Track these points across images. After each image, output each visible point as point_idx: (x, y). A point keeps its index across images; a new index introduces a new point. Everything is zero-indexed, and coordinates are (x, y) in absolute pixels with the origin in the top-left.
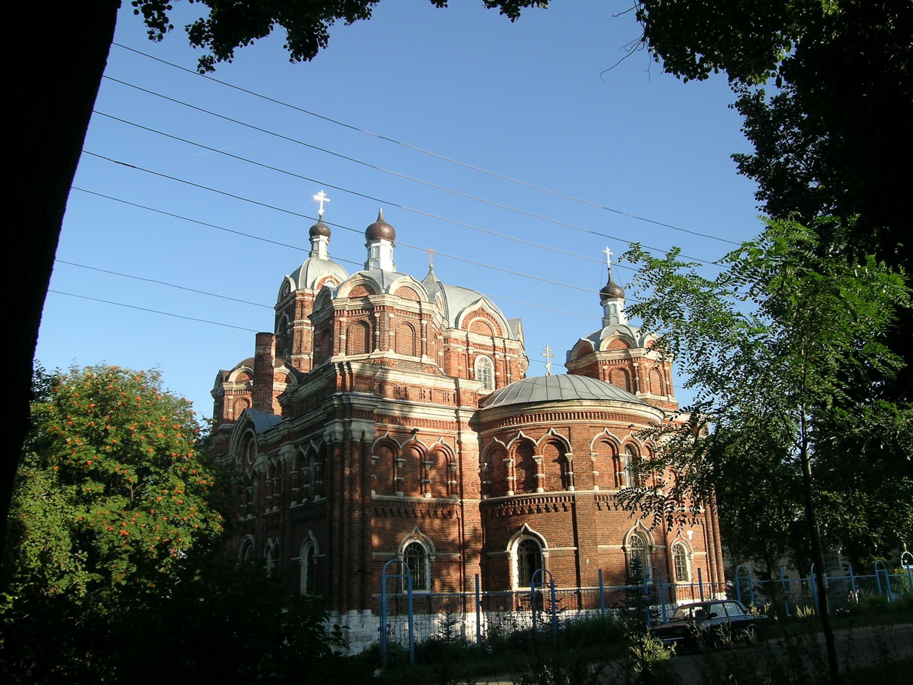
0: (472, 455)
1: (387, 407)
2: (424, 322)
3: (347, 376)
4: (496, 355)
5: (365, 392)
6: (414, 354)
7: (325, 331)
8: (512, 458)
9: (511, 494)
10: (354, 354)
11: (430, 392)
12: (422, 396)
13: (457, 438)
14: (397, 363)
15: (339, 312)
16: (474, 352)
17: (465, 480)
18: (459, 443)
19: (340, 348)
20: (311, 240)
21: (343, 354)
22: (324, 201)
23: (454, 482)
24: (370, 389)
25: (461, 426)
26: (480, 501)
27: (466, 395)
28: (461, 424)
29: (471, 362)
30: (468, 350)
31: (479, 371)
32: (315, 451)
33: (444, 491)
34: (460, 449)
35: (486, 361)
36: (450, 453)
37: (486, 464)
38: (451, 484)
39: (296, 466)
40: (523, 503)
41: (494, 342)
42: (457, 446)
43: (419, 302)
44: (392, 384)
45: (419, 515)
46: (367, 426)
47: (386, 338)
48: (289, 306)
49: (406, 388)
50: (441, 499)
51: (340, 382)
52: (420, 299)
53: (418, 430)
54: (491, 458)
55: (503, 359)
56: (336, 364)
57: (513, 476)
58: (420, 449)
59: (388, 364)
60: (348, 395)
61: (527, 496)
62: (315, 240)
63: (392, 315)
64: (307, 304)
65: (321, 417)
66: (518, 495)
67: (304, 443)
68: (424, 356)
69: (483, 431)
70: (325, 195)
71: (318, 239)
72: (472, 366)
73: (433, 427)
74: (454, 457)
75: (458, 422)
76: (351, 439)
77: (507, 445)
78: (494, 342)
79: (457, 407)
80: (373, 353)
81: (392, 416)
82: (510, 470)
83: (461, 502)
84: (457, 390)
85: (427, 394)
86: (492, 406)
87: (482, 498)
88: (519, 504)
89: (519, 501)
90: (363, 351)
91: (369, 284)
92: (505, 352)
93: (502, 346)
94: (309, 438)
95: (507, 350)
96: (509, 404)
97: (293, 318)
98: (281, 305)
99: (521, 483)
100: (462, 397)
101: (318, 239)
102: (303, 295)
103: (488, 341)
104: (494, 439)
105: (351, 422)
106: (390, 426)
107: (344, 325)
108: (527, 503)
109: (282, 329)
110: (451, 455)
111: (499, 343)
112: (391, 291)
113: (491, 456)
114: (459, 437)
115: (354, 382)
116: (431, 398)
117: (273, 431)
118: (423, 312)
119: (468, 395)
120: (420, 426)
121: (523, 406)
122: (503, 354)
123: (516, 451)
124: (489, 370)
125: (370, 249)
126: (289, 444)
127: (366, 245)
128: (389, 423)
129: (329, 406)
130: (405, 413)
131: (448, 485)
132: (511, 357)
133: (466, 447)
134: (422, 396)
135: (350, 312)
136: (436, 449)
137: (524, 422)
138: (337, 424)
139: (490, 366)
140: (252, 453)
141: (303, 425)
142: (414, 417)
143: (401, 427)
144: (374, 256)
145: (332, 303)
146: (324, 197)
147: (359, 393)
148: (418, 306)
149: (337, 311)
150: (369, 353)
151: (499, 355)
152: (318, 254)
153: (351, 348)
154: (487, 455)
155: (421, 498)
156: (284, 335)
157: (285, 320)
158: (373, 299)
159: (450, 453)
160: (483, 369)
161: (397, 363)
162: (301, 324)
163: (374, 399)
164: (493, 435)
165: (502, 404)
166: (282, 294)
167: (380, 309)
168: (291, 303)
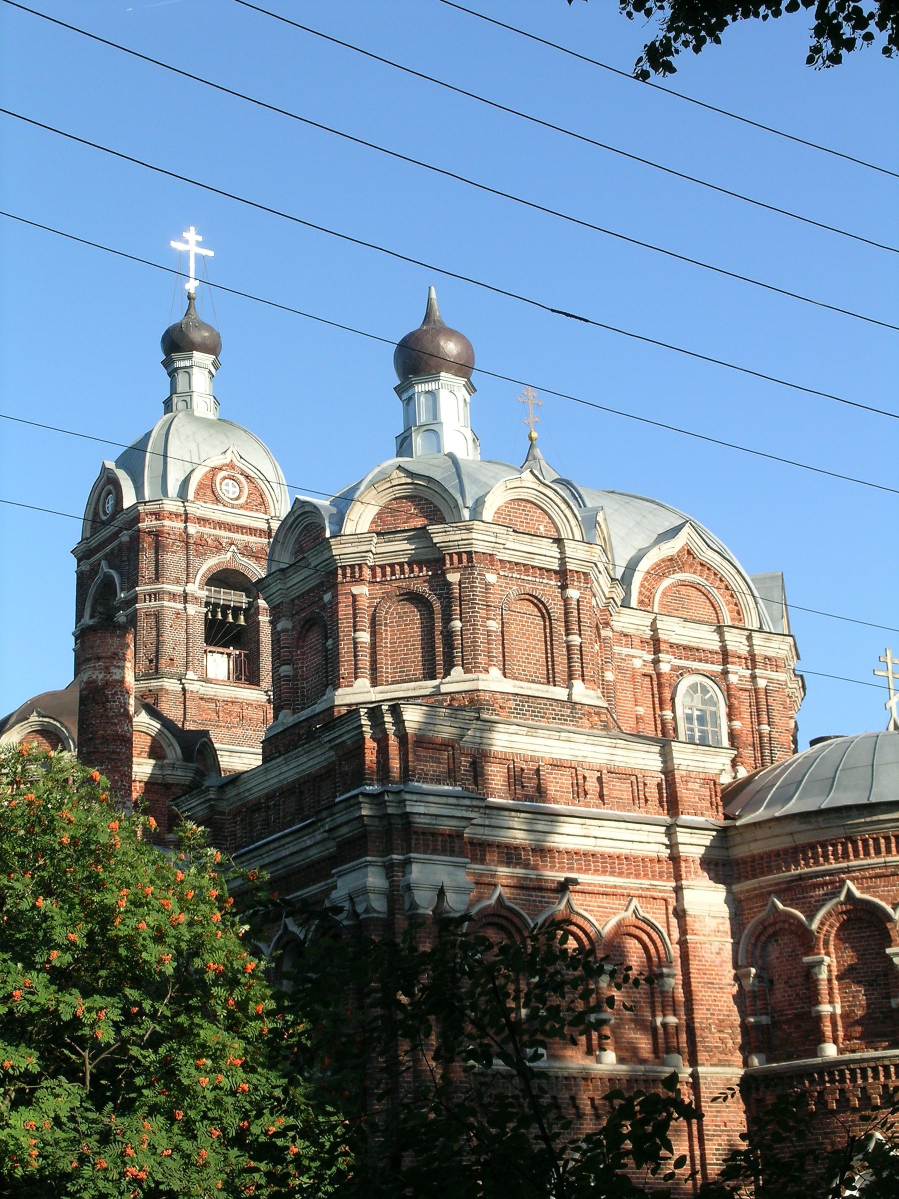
0: (715, 948)
1: (494, 822)
2: (573, 593)
3: (393, 741)
4: (730, 676)
5: (438, 782)
6: (551, 679)
7: (307, 621)
8: (828, 954)
9: (830, 1051)
10: (393, 683)
11: (600, 779)
12: (579, 791)
13: (673, 903)
14: (512, 704)
15: (349, 571)
16: (675, 668)
17: (700, 1015)
18: (680, 914)
20: (167, 363)
21: (363, 683)
22: (198, 257)
23: (672, 1020)
24: (451, 776)
25: (683, 869)
26: (741, 1072)
27: (690, 785)
28: (683, 864)
29: (667, 694)
30: (656, 662)
31: (689, 718)
33: (644, 1044)
34: (683, 931)
35: (705, 690)
36: (658, 941)
37: (753, 970)
38: (665, 1025)
40: (865, 1077)
41: (722, 640)
42: (674, 921)
43: (559, 541)
44: (503, 760)
45: (588, 1110)
46: (449, 874)
47: (481, 638)
49: (538, 770)
50: (642, 1068)
51: (374, 758)
52: (558, 530)
53: (575, 882)
54: (764, 956)
55: (748, 686)
56: (363, 711)
57: (831, 1002)
58: (580, 934)
59: (489, 706)
60: (398, 793)
61: (878, 1059)
62: (179, 364)
63: (491, 578)
65: (313, 852)
66: (848, 1056)
68: (578, 684)
69: (739, 880)
70: (200, 238)
71: (188, 363)
72: (668, 706)
73: (612, 873)
74: (667, 952)
75: (675, 859)
76: (409, 909)
77: (811, 917)
78: (722, 640)
79: (667, 819)
80: (448, 679)
81: (508, 847)
82: (824, 987)
83: (695, 1076)
84: (668, 772)
85: (592, 785)
86: (760, 814)
87: (746, 1063)
88: (854, 1079)
89: (853, 1072)
90: (419, 673)
91: (427, 494)
92: (754, 667)
93: (743, 650)
95: (759, 659)
96: (814, 808)
97: (132, 580)
98: (94, 543)
99: (858, 1023)
100: (682, 792)
101: (188, 363)
102: (158, 515)
103: (707, 639)
104: (774, 906)
105: (408, 862)
106: (503, 871)
107: (363, 603)
108: (876, 1077)
109: (100, 609)
110: (661, 948)
111: (736, 642)
112: (488, 514)
113: (764, 948)
114: (679, 898)
115: (411, 757)
116: (601, 796)
118: (570, 567)
119: (697, 786)
120: (579, 870)
121: (854, 813)
122: (748, 673)
123: (837, 935)
124: (715, 715)
125: (410, 398)
127: (400, 390)
128: (501, 863)
129: (346, 823)
130: (540, 836)
131: (654, 1029)
132: (770, 680)
133: (697, 926)
134: (579, 791)
135: (378, 570)
136: (621, 931)
137: (857, 856)
138: (370, 869)
139: (715, 704)
142: (562, 847)
143: (532, 874)
144: (423, 417)
145: (329, 548)
146: (199, 244)
147: (425, 786)
148: (554, 551)
149: (344, 568)
150: (433, 677)
151: (738, 674)
152: (188, 405)
153: (386, 667)
154: (755, 945)
155: (589, 1063)
157: (108, 587)
158: (440, 535)
159: (658, 941)
160: (696, 713)
161: (512, 704)
162: (156, 595)
163: (467, 802)
164: (769, 894)
165: (793, 806)
167: (460, 561)
168: (125, 537)
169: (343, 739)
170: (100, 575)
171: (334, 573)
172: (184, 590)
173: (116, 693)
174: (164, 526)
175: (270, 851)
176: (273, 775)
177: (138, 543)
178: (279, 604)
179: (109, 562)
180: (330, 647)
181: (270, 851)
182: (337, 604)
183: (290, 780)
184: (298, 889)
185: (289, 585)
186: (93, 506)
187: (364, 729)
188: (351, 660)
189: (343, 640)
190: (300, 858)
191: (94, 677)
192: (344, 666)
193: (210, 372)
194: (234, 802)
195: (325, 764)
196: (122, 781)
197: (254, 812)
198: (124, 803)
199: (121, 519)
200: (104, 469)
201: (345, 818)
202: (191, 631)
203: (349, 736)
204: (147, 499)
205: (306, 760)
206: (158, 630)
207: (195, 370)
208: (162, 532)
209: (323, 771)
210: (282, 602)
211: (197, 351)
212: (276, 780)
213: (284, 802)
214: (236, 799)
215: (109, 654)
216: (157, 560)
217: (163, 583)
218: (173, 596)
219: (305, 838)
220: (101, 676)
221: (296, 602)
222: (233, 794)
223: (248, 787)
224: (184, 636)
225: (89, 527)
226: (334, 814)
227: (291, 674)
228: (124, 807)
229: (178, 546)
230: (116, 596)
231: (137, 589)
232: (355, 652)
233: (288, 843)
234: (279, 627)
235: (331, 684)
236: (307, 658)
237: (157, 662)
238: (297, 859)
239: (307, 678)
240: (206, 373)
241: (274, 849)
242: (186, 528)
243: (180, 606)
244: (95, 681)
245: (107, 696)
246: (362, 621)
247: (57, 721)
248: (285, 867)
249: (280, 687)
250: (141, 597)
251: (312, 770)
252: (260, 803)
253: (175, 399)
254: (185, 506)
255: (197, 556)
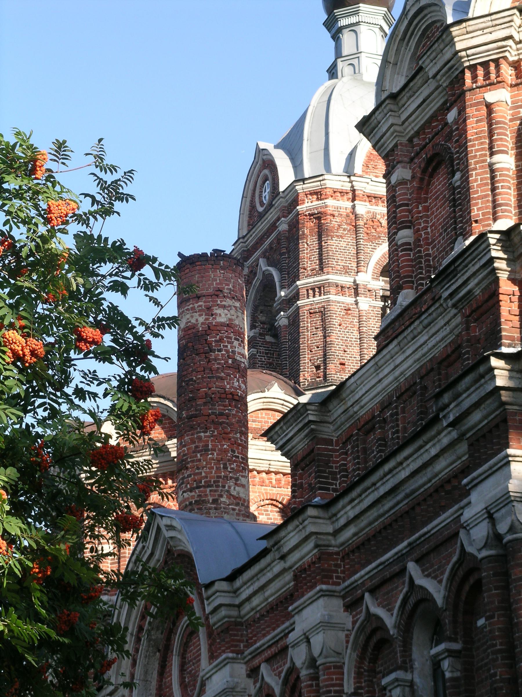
7: (429, 161)
19: (495, 205)
32: (433, 600)
39: (359, 675)
48: (278, 239)
62: (343, 22)
64: (334, 222)
65: (441, 464)
67: (384, 582)
71: (353, 20)
94: (402, 558)
98: (251, 241)
101: (353, 20)
102: (318, 194)
109: (262, 318)
117: (263, 563)
126: (324, 594)
129: (476, 405)
140: (190, 668)
141: (373, 513)
145: (451, 42)
149: (473, 68)
156: (268, 338)
166: (252, 202)
168: (283, 227)
169: (469, 287)
170: (259, 276)
171: (460, 78)
172: (355, 281)
173: (221, 340)
174: (326, 206)
175: (385, 475)
176: (386, 371)
177: (298, 230)
178: (392, 150)
179: (268, 259)
180: (458, 183)
181: (385, 475)
182: (465, 120)
183: (408, 373)
184: (425, 524)
185: (404, 117)
186: (249, 199)
187: (496, 265)
188: (487, 196)
189: (476, 169)
190: (425, 479)
191: (193, 321)
192: (477, 204)
193: (381, 29)
194: (342, 424)
195: (452, 338)
196: (233, 451)
197: (368, 433)
198: (237, 479)
199: (280, 203)
200: (260, 152)
201: (474, 398)
202: (364, 329)
203: (476, 281)
204: (307, 176)
205: (425, 338)
206: (324, 329)
207: (363, 29)
208: (325, 214)
209: (449, 350)
210: (396, 145)
211: (364, 2)
212: (390, 378)
213: (403, 409)
214: (343, 418)
215: (211, 291)
216: (320, 248)
217: (328, 273)
218: (342, 289)
219: (428, 447)
220: (201, 320)
221: (416, 141)
222: (340, 411)
223: (357, 397)
224: (356, 334)
225: (246, 224)
226: (459, 395)
227: (411, 240)
228: (236, 484)
229: (344, 230)
230: (276, 295)
231: (298, 283)
232: (493, 184)
233: (406, 458)
234: (394, 179)
235: (461, 234)
236: (433, 213)
237: (325, 368)
238: (421, 482)
239: (433, 241)
240: (377, 30)
241: (390, 471)
242: (354, 207)
243: (350, 300)
244: (194, 327)
245: (209, 344)
246: (501, 139)
247: (168, 400)
248: (407, 496)
249: (397, 260)
250: (303, 292)
251: (435, 352)
252: (374, 417)
253: (340, 64)
254: (351, 182)
255: (369, 240)
